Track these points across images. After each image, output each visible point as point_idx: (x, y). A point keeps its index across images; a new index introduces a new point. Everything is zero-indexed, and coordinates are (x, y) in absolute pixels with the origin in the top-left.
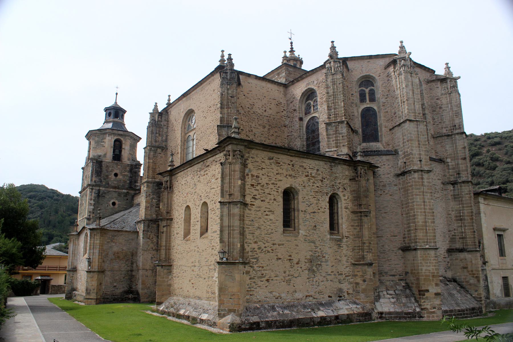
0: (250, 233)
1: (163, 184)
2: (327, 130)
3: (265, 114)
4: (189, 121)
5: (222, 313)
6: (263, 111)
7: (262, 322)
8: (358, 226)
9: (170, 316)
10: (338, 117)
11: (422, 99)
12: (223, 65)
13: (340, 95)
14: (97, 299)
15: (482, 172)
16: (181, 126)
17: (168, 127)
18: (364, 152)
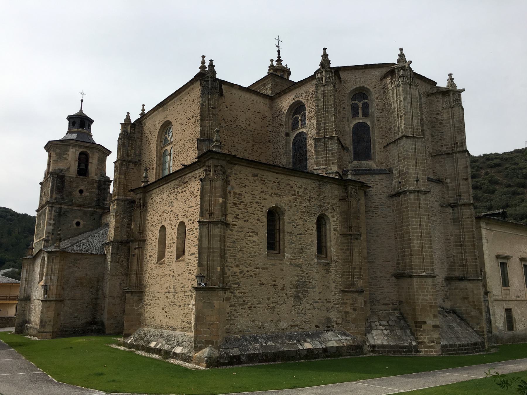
0: (231, 256)
1: (136, 201)
2: (316, 146)
3: (249, 128)
4: (166, 134)
5: (199, 345)
6: (247, 126)
7: (243, 355)
8: (347, 249)
9: (139, 350)
10: (328, 132)
11: (422, 114)
12: (204, 72)
13: (331, 108)
14: (53, 332)
15: (479, 196)
16: (156, 139)
17: (142, 139)
18: (355, 170)
